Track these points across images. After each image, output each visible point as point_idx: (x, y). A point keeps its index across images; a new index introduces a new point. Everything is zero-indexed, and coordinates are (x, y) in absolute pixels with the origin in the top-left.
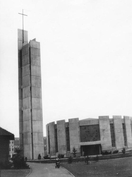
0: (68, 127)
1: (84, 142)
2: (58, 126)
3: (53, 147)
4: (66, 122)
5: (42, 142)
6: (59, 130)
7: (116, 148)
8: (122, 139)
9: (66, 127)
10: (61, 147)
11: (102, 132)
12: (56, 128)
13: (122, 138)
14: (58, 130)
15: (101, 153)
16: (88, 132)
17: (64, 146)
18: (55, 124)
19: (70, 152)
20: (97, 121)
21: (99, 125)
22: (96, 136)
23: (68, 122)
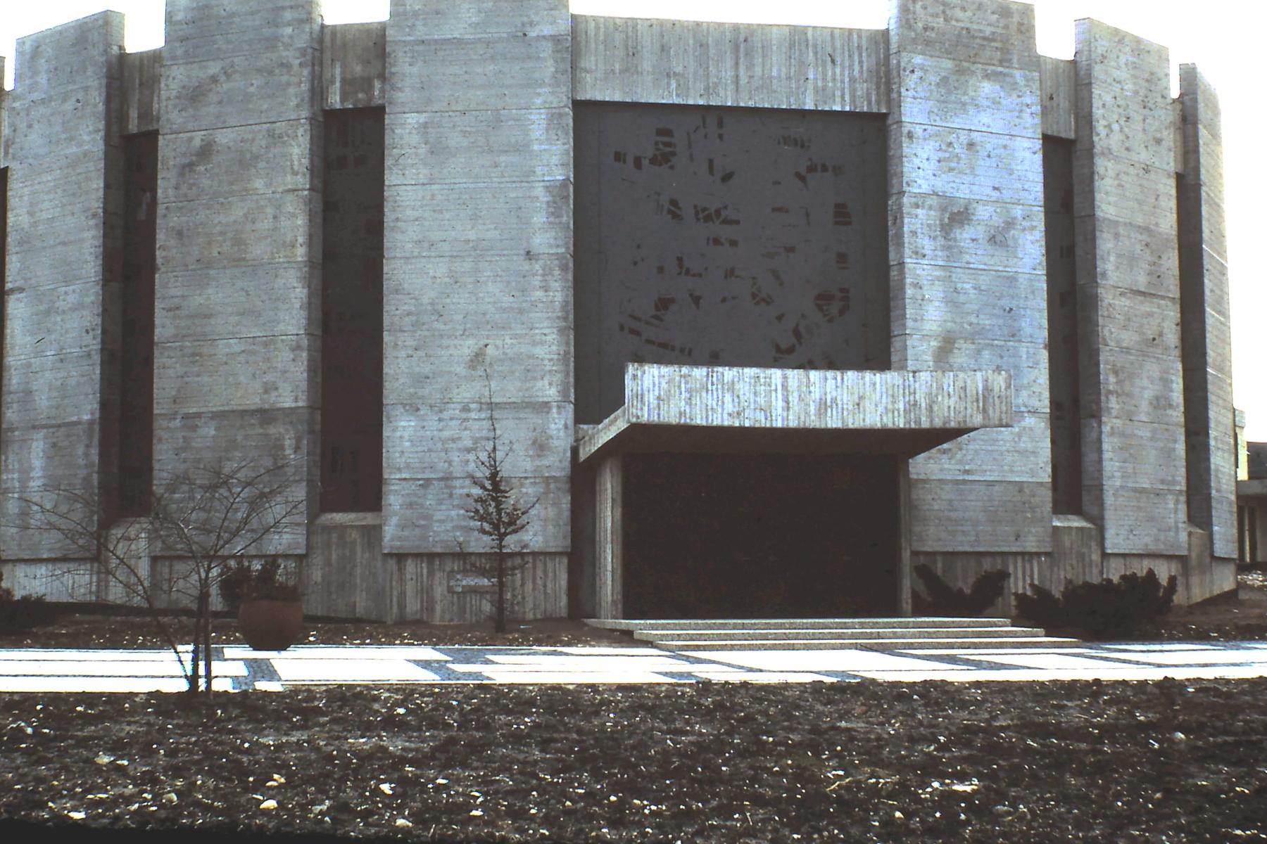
0: (379, 112)
1: (699, 372)
2: (175, 80)
3: (58, 428)
4: (329, 21)
5: (300, 178)
6: (206, 152)
7: (1101, 530)
8: (1160, 403)
9: (335, 100)
10: (209, 431)
11: (927, 245)
12: (146, 114)
13: (1166, 383)
14: (169, 151)
15: (915, 596)
16: (706, 216)
17: (266, 415)
18: (123, 57)
19: (372, 534)
20: (861, 66)
21: (882, 117)
22: (823, 299)
23: (383, 27)
